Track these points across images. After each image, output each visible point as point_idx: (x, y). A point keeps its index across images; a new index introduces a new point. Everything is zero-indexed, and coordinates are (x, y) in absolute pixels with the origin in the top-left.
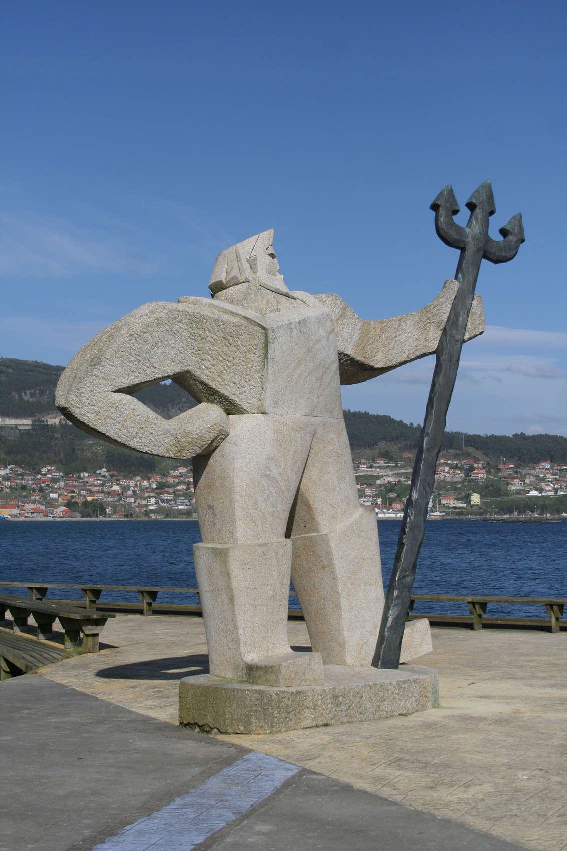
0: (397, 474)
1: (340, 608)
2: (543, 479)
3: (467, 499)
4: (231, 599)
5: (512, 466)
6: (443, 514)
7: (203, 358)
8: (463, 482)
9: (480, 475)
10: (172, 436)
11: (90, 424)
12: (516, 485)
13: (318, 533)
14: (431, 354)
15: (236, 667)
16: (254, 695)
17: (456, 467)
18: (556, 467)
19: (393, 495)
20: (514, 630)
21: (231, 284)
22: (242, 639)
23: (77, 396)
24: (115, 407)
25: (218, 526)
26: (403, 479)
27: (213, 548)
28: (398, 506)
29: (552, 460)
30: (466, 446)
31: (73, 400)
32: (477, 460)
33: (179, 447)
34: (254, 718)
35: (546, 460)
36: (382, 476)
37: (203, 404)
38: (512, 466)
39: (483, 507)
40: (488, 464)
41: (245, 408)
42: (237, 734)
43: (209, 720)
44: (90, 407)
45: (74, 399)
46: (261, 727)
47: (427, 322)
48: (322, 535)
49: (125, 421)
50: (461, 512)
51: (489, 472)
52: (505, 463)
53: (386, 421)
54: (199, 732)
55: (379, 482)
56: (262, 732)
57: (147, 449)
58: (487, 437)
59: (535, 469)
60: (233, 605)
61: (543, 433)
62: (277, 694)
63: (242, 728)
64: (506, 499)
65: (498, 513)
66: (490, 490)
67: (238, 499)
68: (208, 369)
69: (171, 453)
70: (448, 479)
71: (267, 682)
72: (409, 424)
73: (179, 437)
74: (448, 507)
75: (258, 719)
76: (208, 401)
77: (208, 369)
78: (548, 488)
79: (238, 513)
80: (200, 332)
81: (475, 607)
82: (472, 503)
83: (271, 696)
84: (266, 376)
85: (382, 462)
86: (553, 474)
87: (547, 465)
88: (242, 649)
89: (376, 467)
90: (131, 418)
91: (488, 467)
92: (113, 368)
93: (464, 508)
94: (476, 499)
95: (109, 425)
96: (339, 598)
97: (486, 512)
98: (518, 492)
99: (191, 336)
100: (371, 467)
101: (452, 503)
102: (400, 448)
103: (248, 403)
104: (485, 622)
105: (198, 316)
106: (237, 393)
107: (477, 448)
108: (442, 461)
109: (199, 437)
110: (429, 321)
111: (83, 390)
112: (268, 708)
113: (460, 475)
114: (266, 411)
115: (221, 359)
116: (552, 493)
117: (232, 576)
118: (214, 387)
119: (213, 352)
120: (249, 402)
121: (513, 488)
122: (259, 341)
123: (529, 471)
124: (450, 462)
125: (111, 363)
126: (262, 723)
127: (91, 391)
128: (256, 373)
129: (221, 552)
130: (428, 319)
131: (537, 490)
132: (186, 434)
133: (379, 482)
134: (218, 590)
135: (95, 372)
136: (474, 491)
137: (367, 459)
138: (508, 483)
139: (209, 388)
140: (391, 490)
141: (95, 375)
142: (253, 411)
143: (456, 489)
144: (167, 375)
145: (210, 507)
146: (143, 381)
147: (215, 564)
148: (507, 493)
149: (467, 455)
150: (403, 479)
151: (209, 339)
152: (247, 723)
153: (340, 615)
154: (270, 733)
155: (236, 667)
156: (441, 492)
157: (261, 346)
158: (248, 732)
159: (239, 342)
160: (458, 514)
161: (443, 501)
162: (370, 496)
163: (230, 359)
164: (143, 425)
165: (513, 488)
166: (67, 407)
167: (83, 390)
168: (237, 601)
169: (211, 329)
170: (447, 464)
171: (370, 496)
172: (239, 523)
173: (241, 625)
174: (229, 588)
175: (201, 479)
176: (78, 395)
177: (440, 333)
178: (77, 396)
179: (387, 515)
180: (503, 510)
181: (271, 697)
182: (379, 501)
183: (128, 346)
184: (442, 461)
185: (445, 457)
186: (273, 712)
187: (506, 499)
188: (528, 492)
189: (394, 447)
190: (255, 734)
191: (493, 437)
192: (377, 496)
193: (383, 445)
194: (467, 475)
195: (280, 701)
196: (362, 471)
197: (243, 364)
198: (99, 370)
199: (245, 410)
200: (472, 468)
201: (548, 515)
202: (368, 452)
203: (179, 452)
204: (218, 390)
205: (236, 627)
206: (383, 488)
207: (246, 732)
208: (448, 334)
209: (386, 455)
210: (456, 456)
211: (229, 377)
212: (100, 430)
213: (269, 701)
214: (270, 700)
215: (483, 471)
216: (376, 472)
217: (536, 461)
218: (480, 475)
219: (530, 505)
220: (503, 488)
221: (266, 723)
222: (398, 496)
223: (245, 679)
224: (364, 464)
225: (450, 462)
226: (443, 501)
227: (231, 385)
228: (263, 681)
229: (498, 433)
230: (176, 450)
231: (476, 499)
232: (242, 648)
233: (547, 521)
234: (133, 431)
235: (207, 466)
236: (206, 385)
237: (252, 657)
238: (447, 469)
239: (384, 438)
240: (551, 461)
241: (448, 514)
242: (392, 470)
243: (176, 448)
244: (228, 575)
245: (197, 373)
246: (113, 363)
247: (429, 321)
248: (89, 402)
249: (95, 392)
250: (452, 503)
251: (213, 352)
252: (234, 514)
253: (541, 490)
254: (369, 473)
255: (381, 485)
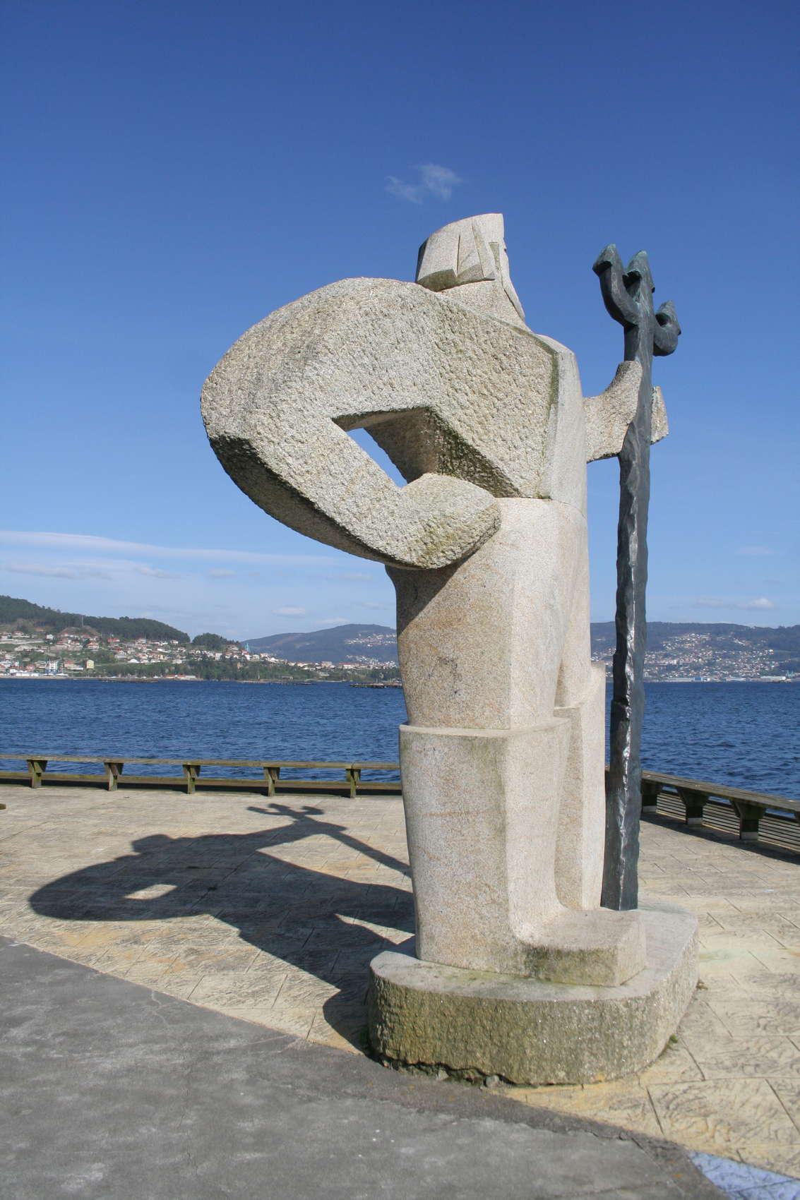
0: (30, 644)
1: (580, 825)
2: (141, 651)
3: (84, 664)
4: (501, 831)
5: (118, 641)
6: (66, 675)
7: (457, 386)
8: (81, 652)
9: (95, 647)
10: (421, 521)
11: (292, 482)
12: (120, 655)
13: (561, 706)
14: (613, 455)
15: (498, 950)
16: (587, 1011)
17: (76, 640)
18: (150, 642)
19: (27, 660)
20: (389, 797)
21: (466, 279)
22: (513, 899)
23: (272, 417)
24: (337, 451)
25: (463, 696)
26: (35, 648)
27: (465, 738)
28: (31, 668)
29: (148, 637)
30: (84, 624)
31: (263, 424)
32: (92, 635)
33: (430, 545)
34: (587, 1053)
35: (143, 637)
36: (19, 645)
37: (426, 476)
38: (118, 641)
39: (97, 670)
40: (101, 639)
41: (516, 485)
42: (551, 1084)
43: (482, 1060)
44: (295, 443)
45: (266, 423)
46: (602, 1069)
47: (612, 411)
48: (568, 710)
49: (352, 482)
50: (78, 674)
51: (101, 645)
52: (113, 638)
53: (24, 603)
54: (446, 1080)
55: (16, 649)
56: (602, 1079)
57: (380, 544)
58: (101, 619)
59: (134, 643)
60: (504, 842)
61: (154, 619)
62: (627, 1005)
63: (562, 1074)
64: (113, 665)
65: (107, 675)
66: (100, 657)
67: (518, 648)
68: (462, 407)
69: (414, 554)
70: (70, 649)
71: (587, 981)
72: (41, 607)
73: (433, 525)
74: (70, 670)
75: (595, 1055)
76: (445, 469)
77: (462, 407)
78: (144, 657)
79: (515, 673)
80: (457, 337)
81: (352, 775)
82: (88, 667)
83: (618, 1009)
84: (552, 433)
85: (19, 635)
86: (148, 648)
87: (144, 641)
88: (514, 918)
89: (14, 638)
90: (363, 477)
91: (101, 641)
92: (336, 371)
93: (81, 671)
94: (90, 664)
95: (324, 486)
96: (580, 809)
97: (97, 674)
98: (122, 660)
99: (440, 344)
100: (11, 638)
101: (73, 667)
102: (34, 625)
103: (522, 477)
104: (360, 787)
105: (455, 309)
106: (507, 457)
107: (93, 627)
108: (66, 635)
109: (466, 528)
110: (614, 410)
111: (285, 406)
112: (613, 1034)
113: (79, 646)
114: (551, 495)
115: (486, 392)
116: (147, 661)
117: (507, 789)
118: (470, 442)
119: (474, 379)
120: (524, 475)
121: (118, 657)
122: (546, 370)
123: (131, 645)
124: (72, 636)
125: (335, 360)
126: (603, 1062)
127: (300, 410)
128: (538, 425)
129: (486, 746)
130: (614, 407)
131: (136, 658)
132: (446, 520)
133: (16, 649)
134: (468, 813)
135: (309, 371)
136: (89, 658)
137: (8, 632)
138: (115, 654)
139: (457, 444)
140: (26, 656)
141: (308, 378)
142: (528, 492)
143: (75, 656)
144: (405, 407)
145: (443, 661)
146: (376, 409)
147: (465, 766)
148: (114, 661)
149: (85, 632)
150: (35, 648)
151: (470, 353)
152: (573, 1065)
153: (578, 835)
154: (617, 1078)
155: (498, 950)
156: (64, 658)
157: (547, 380)
158: (575, 1079)
159: (517, 367)
160: (77, 675)
161: (66, 666)
162: (9, 660)
163: (501, 395)
164: (380, 495)
165: (118, 657)
166: (247, 438)
167: (285, 406)
168: (510, 834)
169: (474, 336)
170: (69, 638)
171: (9, 660)
172: (515, 691)
173: (512, 875)
174: (498, 811)
175: (425, 610)
176: (274, 415)
177: (626, 428)
178: (272, 417)
179: (23, 675)
180: (110, 673)
181: (618, 1012)
182: (17, 664)
183: (361, 332)
184: (66, 635)
185: (67, 632)
186: (622, 1039)
187: (113, 665)
188: (130, 660)
189: (30, 624)
190: (589, 1083)
191: (105, 619)
192: (15, 660)
193: (21, 621)
194: (85, 646)
195: (632, 1017)
196: (4, 641)
197: (520, 406)
198: (315, 368)
199: (516, 490)
200: (89, 642)
201: (145, 677)
202: (9, 626)
203: (428, 554)
204: (476, 448)
205: (503, 879)
206: (19, 654)
207: (572, 1081)
208: (637, 431)
209: (24, 629)
210: (77, 632)
211: (496, 427)
212: (308, 496)
213: (615, 1019)
214: (617, 1016)
215: (97, 644)
216: (15, 642)
217: (135, 637)
218: (95, 647)
219: (131, 670)
220: (110, 657)
221: (609, 1060)
222: (31, 660)
223: (524, 972)
224: (5, 635)
225: (72, 636)
226: (66, 666)
227: (499, 441)
228: (574, 978)
229: (109, 616)
230: (422, 550)
231: (90, 664)
232: (511, 916)
233: (143, 682)
234: (365, 504)
235: (447, 586)
236: (456, 437)
237: (528, 931)
238: (69, 641)
239: (22, 617)
240: (147, 638)
241: (70, 675)
242: (27, 641)
243: (424, 547)
244: (500, 787)
245: (445, 414)
246: (338, 360)
247: (614, 410)
248: (293, 432)
249: (306, 413)
250: (73, 667)
251: (474, 379)
252: (507, 675)
253: (139, 659)
254: (9, 643)
255: (18, 652)
